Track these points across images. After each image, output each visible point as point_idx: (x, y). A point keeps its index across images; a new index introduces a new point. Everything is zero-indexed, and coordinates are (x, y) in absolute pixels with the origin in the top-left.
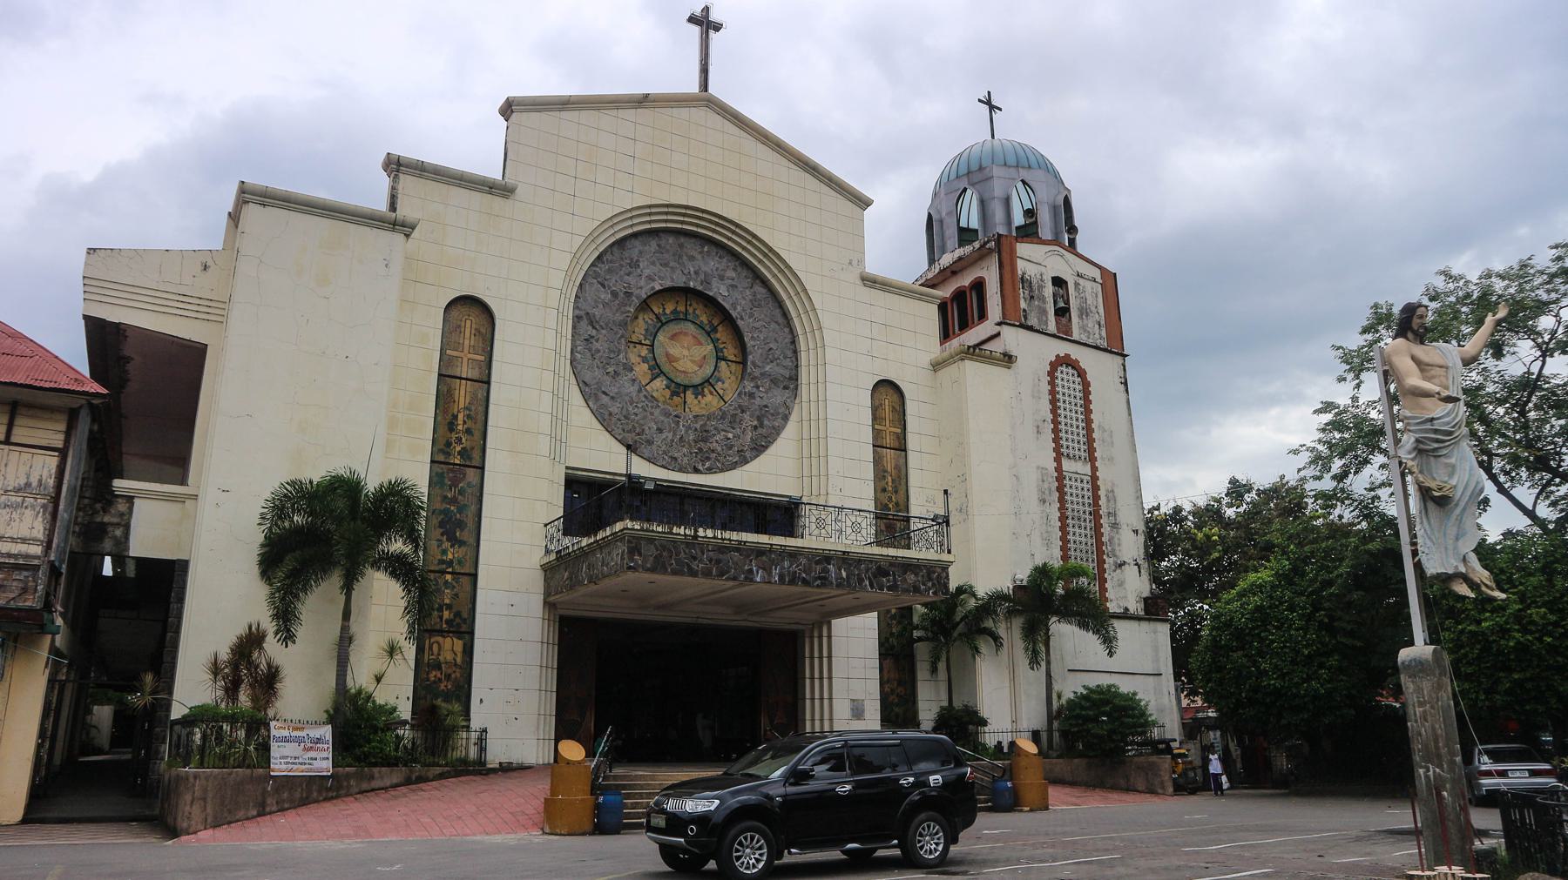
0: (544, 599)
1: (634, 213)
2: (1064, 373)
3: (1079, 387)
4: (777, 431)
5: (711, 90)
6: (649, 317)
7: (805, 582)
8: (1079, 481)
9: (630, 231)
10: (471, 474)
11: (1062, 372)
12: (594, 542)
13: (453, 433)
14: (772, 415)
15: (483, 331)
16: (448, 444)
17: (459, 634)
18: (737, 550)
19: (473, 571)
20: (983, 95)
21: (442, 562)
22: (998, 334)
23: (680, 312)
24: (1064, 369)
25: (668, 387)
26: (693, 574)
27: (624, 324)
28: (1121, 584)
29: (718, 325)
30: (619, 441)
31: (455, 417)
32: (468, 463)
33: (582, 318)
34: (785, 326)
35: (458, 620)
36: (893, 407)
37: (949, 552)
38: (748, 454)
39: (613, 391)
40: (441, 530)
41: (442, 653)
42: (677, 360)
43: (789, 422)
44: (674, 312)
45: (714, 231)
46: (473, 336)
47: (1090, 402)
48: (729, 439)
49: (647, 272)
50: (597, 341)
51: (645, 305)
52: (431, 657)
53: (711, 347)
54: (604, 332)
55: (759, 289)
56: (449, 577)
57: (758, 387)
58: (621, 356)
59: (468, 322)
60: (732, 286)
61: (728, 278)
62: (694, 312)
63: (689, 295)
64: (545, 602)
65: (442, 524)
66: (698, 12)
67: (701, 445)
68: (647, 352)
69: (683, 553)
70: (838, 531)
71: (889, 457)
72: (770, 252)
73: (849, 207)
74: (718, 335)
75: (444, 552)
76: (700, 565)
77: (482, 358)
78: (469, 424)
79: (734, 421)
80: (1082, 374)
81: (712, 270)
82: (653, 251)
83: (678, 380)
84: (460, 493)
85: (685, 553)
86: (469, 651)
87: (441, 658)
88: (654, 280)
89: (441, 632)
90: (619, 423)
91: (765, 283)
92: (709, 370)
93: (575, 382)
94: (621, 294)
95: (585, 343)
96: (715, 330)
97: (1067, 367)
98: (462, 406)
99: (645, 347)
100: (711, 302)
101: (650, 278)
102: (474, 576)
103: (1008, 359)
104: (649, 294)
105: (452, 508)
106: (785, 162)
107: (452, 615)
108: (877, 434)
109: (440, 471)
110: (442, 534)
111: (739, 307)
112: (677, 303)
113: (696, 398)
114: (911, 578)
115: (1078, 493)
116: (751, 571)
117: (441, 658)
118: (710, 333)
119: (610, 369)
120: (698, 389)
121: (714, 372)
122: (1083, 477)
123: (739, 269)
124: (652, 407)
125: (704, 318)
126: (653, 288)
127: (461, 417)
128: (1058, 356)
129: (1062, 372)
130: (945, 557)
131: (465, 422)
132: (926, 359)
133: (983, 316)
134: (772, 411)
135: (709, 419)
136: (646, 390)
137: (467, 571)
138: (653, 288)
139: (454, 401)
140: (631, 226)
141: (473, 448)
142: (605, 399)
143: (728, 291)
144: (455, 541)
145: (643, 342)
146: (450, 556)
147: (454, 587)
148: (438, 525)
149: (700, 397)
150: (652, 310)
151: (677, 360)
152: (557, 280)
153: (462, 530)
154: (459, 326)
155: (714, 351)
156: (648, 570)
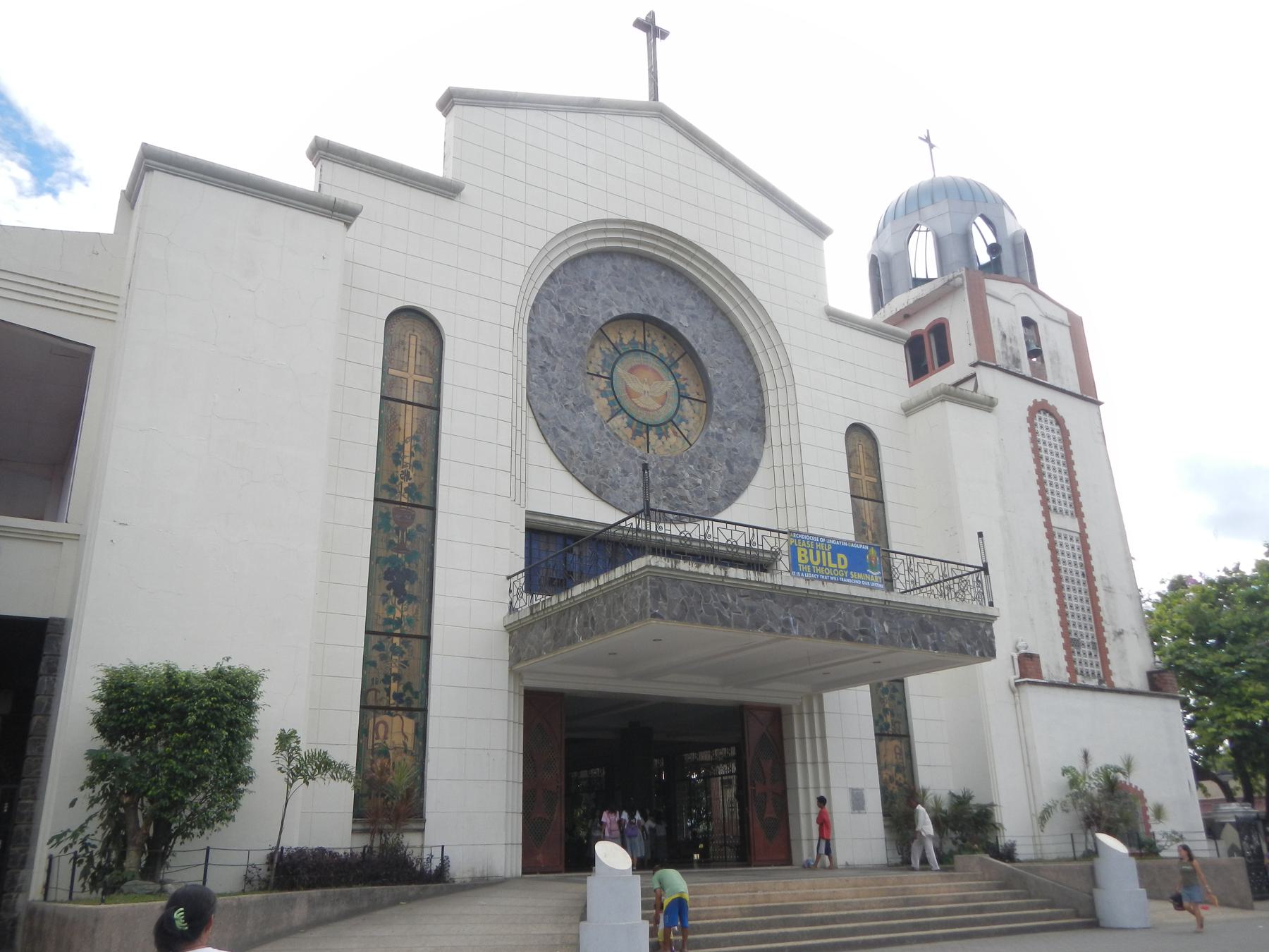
0: (511, 667)
1: (590, 228)
2: (1043, 421)
3: (1058, 436)
4: (748, 478)
5: (661, 100)
6: (606, 346)
7: (847, 638)
8: (1069, 538)
9: (583, 249)
10: (421, 516)
11: (1040, 419)
12: (596, 588)
13: (399, 467)
14: (741, 459)
15: (431, 349)
16: (394, 479)
17: (410, 711)
18: (772, 595)
19: (425, 634)
20: (924, 135)
21: (388, 621)
22: (974, 375)
23: (638, 343)
24: (1042, 415)
25: (629, 425)
26: (725, 623)
27: (580, 353)
28: (1123, 654)
29: (679, 359)
30: (582, 483)
31: (401, 448)
32: (417, 502)
33: (537, 343)
34: (749, 363)
35: (408, 694)
36: (868, 454)
37: (991, 604)
38: (720, 502)
39: (573, 426)
40: (387, 583)
41: (389, 735)
42: (638, 395)
43: (760, 469)
44: (632, 342)
45: (672, 254)
46: (418, 355)
47: (1071, 453)
48: (699, 485)
49: (604, 295)
50: (553, 369)
51: (602, 333)
52: (376, 742)
53: (672, 382)
54: (560, 359)
55: (718, 320)
56: (396, 640)
57: (725, 428)
58: (579, 388)
59: (413, 339)
60: (693, 316)
61: (687, 308)
62: (653, 344)
63: (647, 324)
64: (511, 670)
65: (388, 575)
66: (643, 17)
67: (670, 490)
68: (605, 385)
69: (712, 599)
70: (912, 571)
71: (867, 508)
72: (733, 280)
73: (808, 235)
74: (679, 371)
75: (391, 609)
76: (733, 614)
77: (430, 380)
78: (418, 456)
79: (704, 467)
80: (1059, 422)
81: (671, 298)
82: (608, 273)
83: (640, 419)
84: (408, 538)
85: (715, 599)
86: (421, 733)
87: (388, 742)
88: (611, 305)
89: (388, 709)
90: (582, 462)
91: (725, 315)
92: (670, 408)
93: (531, 415)
94: (577, 320)
95: (540, 370)
96: (675, 363)
97: (1044, 413)
98: (408, 434)
99: (603, 380)
100: (671, 333)
101: (606, 304)
102: (427, 639)
103: (988, 405)
104: (607, 320)
105: (400, 556)
106: (742, 183)
107: (401, 689)
108: (853, 483)
109: (384, 511)
110: (389, 588)
111: (700, 339)
112: (635, 332)
113: (660, 438)
114: (955, 635)
115: (1069, 549)
116: (787, 622)
117: (388, 742)
118: (670, 367)
119: (570, 402)
120: (641, 428)
121: (676, 411)
122: (1072, 534)
123: (698, 298)
124: (615, 446)
125: (663, 351)
126: (610, 314)
127: (407, 447)
128: (1035, 401)
129: (1040, 419)
130: (989, 611)
131: (412, 454)
132: (897, 403)
133: (945, 358)
134: (741, 456)
135: (676, 462)
136: (608, 426)
137: (419, 634)
138: (610, 314)
139: (400, 429)
140: (585, 243)
141: (422, 485)
142: (565, 435)
143: (689, 322)
144: (401, 595)
145: (601, 374)
146: (398, 614)
147: (403, 653)
148: (382, 576)
149: (664, 438)
150: (608, 339)
151: (638, 395)
152: (512, 295)
153: (412, 583)
154: (403, 343)
155: (675, 387)
156: (674, 618)
